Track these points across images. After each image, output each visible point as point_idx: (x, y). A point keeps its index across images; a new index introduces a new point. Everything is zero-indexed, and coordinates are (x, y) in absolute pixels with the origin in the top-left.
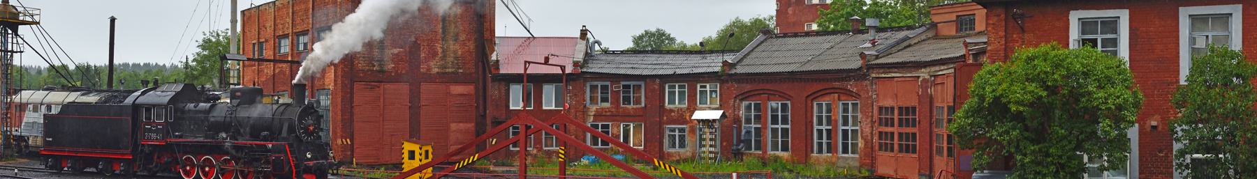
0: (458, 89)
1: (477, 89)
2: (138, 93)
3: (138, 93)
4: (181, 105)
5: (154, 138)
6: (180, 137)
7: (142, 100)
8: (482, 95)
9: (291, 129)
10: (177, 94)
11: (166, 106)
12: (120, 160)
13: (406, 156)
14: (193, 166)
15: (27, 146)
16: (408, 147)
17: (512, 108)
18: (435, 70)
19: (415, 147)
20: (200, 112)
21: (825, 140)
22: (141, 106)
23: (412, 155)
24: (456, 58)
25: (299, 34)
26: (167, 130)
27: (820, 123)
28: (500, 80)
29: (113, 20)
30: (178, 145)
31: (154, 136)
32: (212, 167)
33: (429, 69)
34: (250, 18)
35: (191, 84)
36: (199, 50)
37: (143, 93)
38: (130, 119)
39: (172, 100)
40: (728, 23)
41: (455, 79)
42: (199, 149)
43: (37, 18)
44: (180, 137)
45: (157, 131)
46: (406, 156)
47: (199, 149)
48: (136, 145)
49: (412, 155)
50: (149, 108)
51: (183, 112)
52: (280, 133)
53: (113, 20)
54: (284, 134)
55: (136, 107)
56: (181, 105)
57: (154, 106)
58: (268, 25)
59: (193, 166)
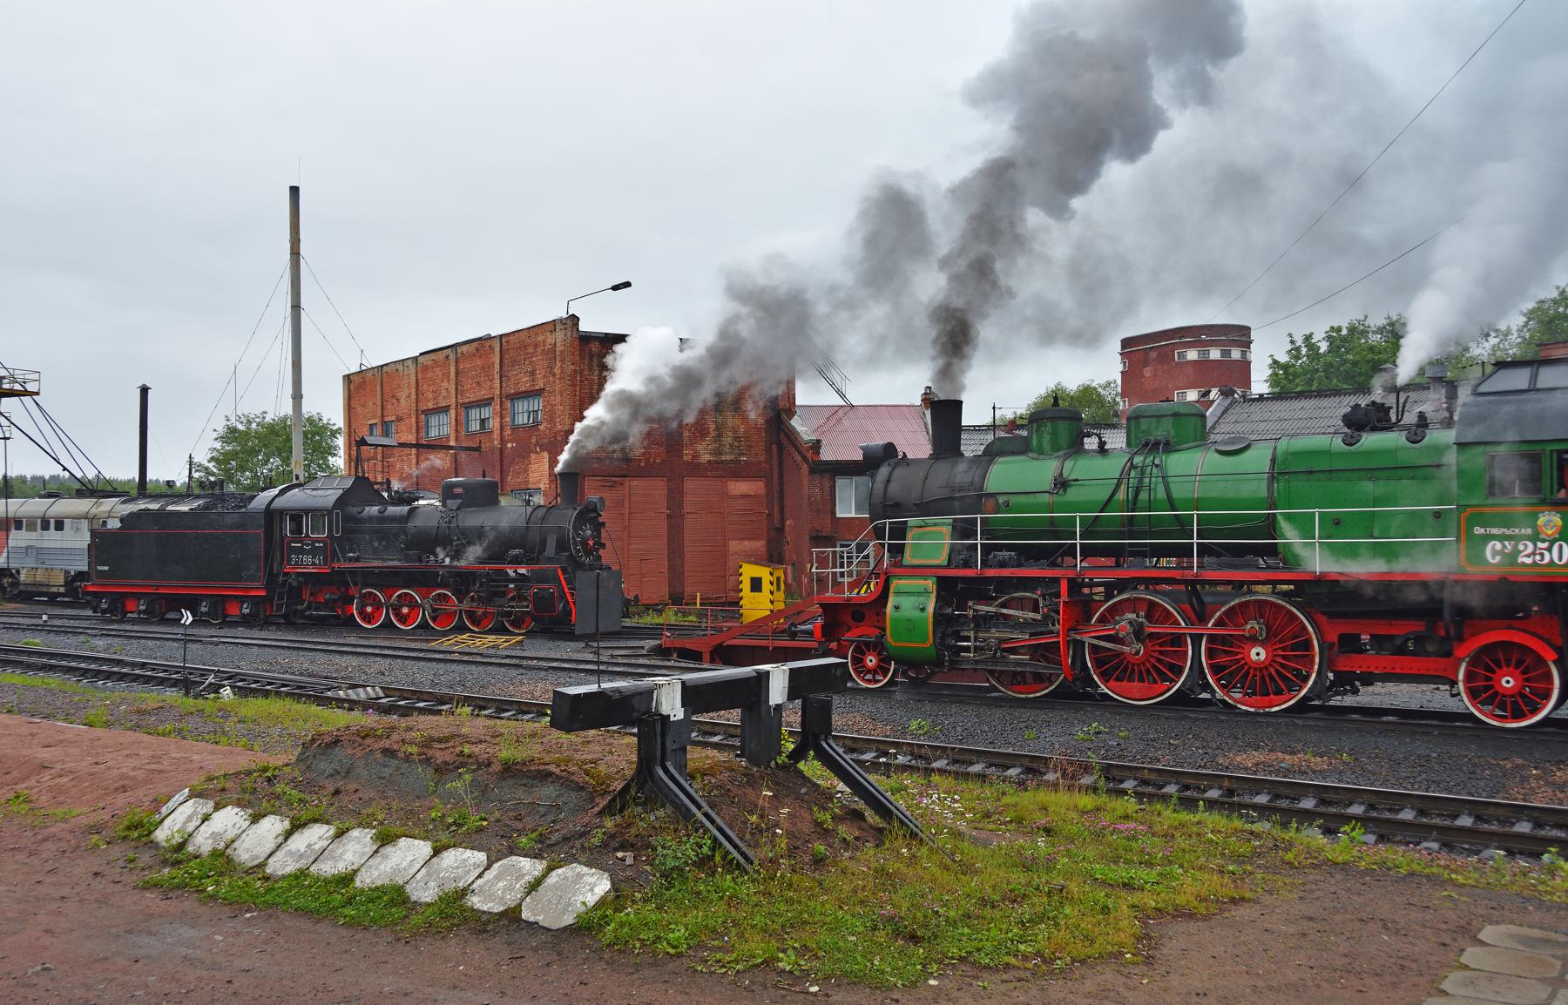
0: (740, 487)
1: (768, 486)
2: (276, 491)
3: (276, 491)
4: (355, 510)
5: (309, 564)
6: (357, 560)
7: (278, 504)
8: (778, 496)
9: (562, 545)
10: (346, 493)
11: (329, 512)
12: (241, 600)
13: (746, 586)
14: (378, 606)
15: (16, 584)
16: (749, 571)
17: (839, 515)
18: (705, 458)
19: (763, 572)
20: (393, 519)
21: (699, 815)
22: (282, 512)
23: (756, 585)
24: (737, 438)
25: (469, 406)
26: (331, 549)
27: (1186, 551)
28: (822, 472)
29: (144, 391)
30: (353, 572)
31: (307, 559)
32: (414, 606)
33: (696, 456)
34: (362, 385)
35: (207, 488)
36: (218, 445)
37: (282, 492)
38: (261, 532)
39: (341, 502)
40: (1043, 392)
41: (737, 471)
42: (388, 580)
43: (31, 387)
44: (357, 560)
45: (314, 552)
46: (746, 586)
47: (388, 580)
48: (272, 577)
49: (756, 585)
50: (297, 515)
51: (357, 520)
52: (543, 550)
53: (144, 391)
54: (550, 550)
55: (272, 515)
56: (355, 510)
57: (307, 511)
58: (403, 395)
59: (378, 606)
